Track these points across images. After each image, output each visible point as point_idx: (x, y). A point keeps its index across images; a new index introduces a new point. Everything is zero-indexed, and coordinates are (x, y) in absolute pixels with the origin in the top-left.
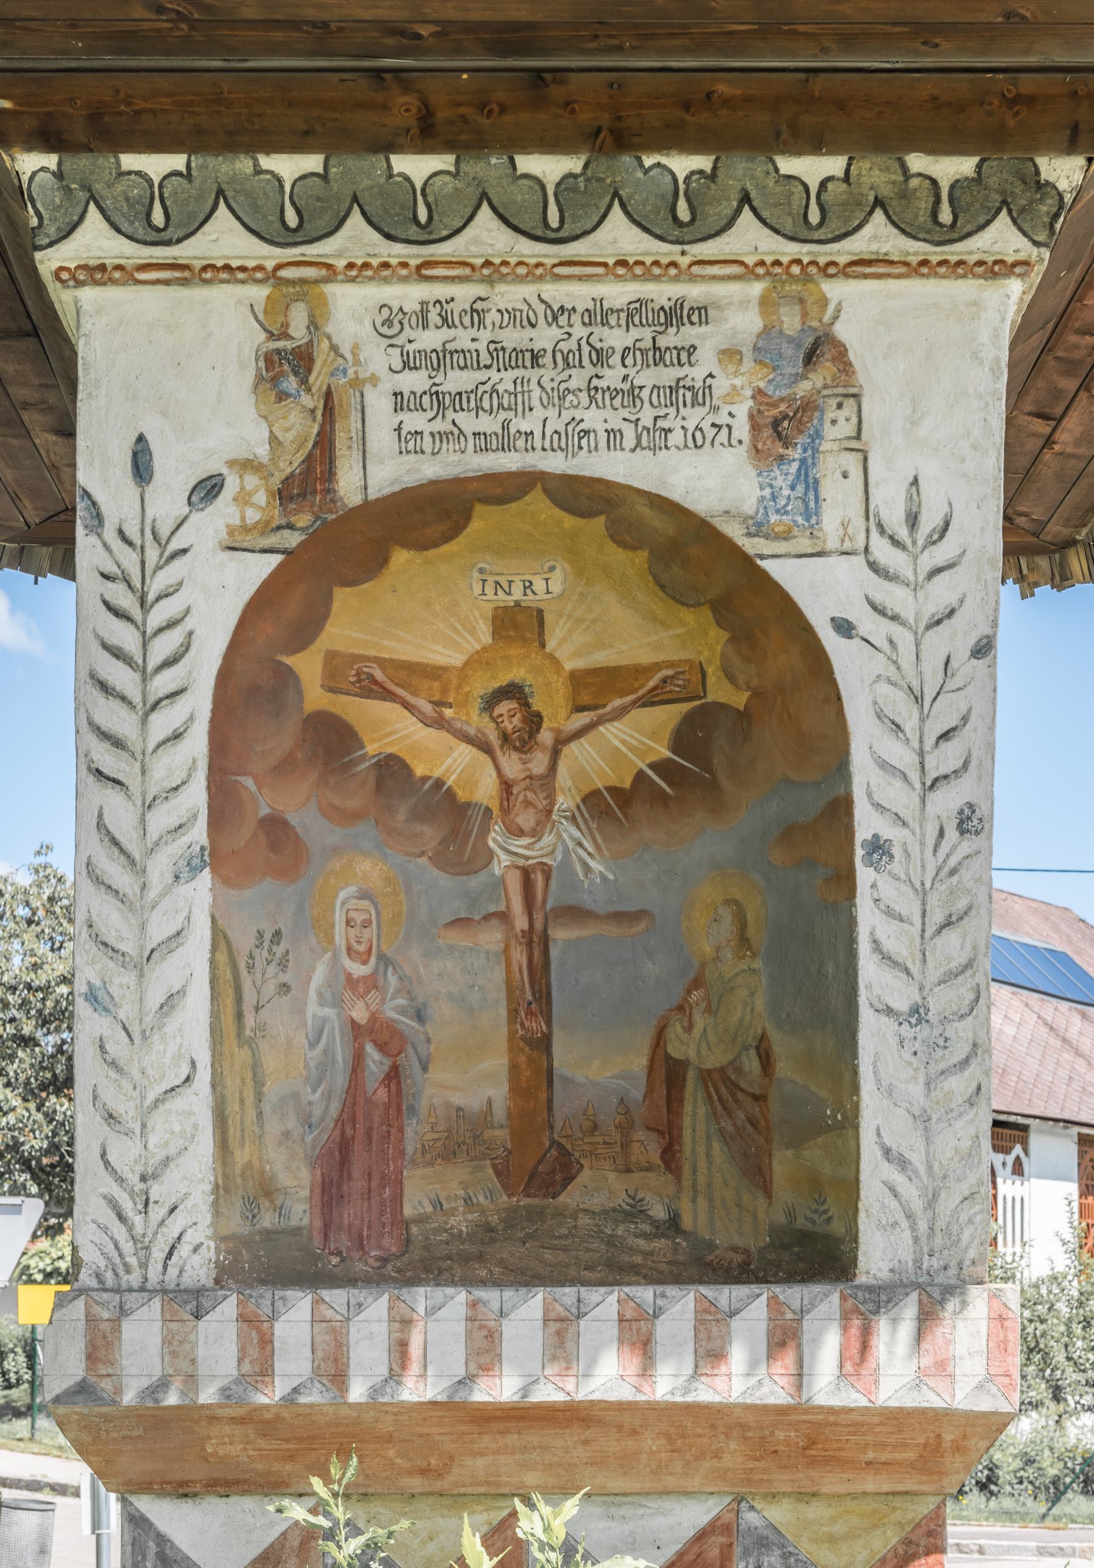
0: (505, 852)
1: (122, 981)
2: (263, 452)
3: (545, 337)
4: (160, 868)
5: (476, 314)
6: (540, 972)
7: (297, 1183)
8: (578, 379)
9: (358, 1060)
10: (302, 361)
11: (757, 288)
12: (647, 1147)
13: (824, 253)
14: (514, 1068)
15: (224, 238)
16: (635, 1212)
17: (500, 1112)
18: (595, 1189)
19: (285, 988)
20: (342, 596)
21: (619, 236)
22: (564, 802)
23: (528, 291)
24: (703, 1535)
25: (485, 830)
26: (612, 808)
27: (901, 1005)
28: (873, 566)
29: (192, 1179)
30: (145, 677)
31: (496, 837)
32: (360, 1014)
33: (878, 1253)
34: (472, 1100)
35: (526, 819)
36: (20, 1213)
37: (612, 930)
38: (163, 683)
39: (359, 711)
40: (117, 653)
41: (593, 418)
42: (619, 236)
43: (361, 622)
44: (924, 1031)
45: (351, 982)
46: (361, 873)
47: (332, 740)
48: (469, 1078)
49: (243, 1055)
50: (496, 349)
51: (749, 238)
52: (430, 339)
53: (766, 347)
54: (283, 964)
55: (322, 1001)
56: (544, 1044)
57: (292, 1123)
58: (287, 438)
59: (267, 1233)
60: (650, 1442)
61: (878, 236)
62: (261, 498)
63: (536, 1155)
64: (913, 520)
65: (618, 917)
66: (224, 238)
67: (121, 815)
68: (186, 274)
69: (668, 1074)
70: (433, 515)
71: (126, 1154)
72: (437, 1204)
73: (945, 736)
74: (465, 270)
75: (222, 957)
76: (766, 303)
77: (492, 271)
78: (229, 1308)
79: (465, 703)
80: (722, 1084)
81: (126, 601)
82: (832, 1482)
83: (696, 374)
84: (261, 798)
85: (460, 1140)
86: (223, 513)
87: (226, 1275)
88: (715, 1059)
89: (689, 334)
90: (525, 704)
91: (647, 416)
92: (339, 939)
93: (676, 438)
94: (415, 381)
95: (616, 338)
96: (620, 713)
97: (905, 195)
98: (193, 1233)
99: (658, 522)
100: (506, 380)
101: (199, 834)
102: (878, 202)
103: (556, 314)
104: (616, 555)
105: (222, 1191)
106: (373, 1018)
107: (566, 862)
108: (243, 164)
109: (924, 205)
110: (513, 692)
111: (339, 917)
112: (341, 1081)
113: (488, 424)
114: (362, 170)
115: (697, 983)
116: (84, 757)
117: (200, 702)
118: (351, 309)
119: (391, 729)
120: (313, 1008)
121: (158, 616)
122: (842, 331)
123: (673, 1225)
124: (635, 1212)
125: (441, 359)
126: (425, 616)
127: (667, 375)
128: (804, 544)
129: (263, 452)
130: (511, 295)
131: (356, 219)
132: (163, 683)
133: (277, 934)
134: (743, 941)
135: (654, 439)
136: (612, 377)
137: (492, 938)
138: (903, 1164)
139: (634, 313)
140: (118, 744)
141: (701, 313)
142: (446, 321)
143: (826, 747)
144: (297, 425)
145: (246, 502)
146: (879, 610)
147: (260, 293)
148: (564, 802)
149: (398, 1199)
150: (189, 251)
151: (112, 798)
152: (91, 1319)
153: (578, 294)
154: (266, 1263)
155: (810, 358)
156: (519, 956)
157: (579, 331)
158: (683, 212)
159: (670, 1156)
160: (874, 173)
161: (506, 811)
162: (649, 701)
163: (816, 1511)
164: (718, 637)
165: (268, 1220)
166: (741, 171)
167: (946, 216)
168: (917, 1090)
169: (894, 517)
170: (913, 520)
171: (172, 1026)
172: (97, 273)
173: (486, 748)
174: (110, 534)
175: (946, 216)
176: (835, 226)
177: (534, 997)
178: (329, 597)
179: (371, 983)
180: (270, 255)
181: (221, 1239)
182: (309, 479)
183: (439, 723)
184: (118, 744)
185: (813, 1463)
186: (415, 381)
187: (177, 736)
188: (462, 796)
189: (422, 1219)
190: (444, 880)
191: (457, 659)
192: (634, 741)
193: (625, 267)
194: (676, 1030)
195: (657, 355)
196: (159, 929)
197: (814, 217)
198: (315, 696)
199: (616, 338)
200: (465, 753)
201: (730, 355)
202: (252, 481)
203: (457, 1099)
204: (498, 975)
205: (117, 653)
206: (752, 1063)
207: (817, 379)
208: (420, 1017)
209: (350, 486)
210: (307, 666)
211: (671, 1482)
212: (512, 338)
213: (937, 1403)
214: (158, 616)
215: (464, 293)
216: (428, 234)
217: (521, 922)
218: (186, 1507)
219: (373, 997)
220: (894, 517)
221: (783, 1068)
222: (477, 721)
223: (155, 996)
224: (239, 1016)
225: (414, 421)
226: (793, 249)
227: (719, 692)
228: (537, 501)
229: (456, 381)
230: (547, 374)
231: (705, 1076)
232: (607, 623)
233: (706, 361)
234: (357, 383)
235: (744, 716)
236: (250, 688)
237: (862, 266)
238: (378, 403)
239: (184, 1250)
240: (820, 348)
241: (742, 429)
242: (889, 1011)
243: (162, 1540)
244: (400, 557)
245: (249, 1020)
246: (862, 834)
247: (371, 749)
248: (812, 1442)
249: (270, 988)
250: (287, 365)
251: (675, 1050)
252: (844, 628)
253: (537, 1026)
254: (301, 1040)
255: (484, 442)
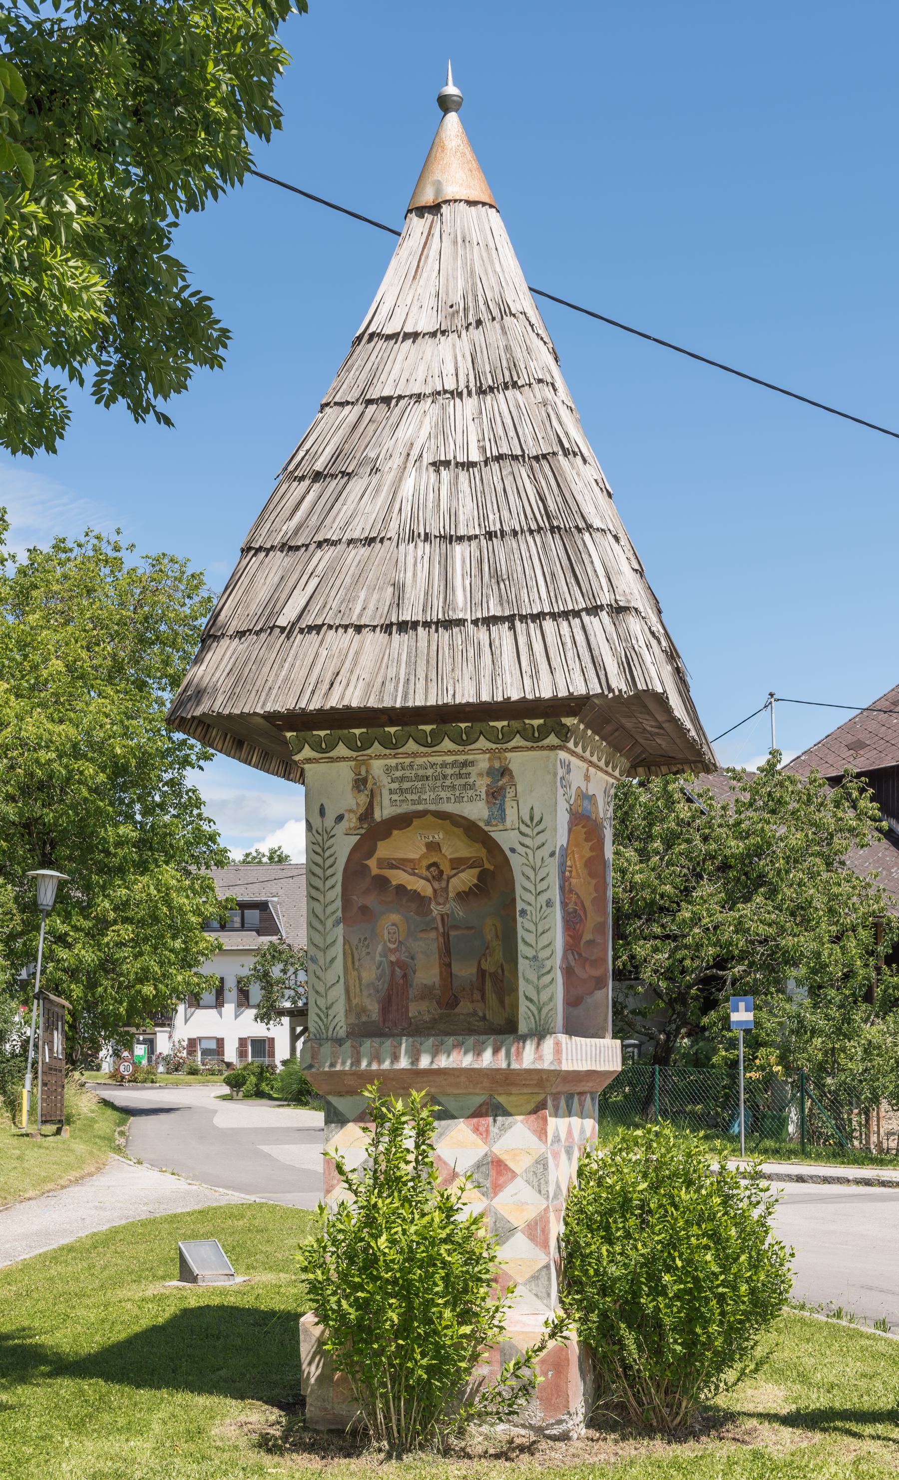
0: (436, 910)
1: (320, 955)
2: (355, 807)
3: (430, 772)
4: (329, 923)
5: (411, 766)
6: (447, 944)
7: (374, 1008)
8: (439, 783)
9: (393, 973)
10: (364, 781)
11: (488, 756)
12: (477, 995)
13: (504, 746)
14: (441, 972)
15: (341, 750)
16: (475, 1014)
17: (437, 985)
18: (465, 1007)
19: (368, 953)
20: (379, 844)
21: (447, 744)
22: (452, 895)
23: (425, 759)
24: (481, 1106)
25: (430, 904)
26: (462, 896)
27: (530, 955)
28: (521, 833)
29: (340, 1008)
30: (324, 871)
31: (433, 906)
32: (393, 959)
33: (523, 1028)
34: (428, 982)
35: (441, 900)
36: (223, 1039)
37: (465, 932)
38: (329, 872)
39: (387, 873)
40: (317, 864)
41: (443, 794)
42: (447, 744)
43: (384, 850)
44: (537, 963)
45: (390, 950)
46: (392, 921)
47: (382, 883)
48: (427, 974)
49: (355, 973)
50: (417, 776)
51: (483, 743)
52: (399, 774)
53: (490, 772)
54: (367, 947)
55: (381, 956)
56: (449, 965)
57: (372, 991)
58: (361, 803)
59: (364, 1023)
60: (463, 1079)
61: (518, 741)
62: (354, 820)
63: (448, 997)
64: (532, 819)
65: (467, 928)
66: (341, 750)
67: (319, 910)
68: (332, 760)
69: (482, 973)
70: (403, 821)
71: (322, 1002)
72: (419, 1013)
73: (542, 880)
74: (408, 755)
75: (347, 947)
76: (490, 759)
77: (415, 755)
78: (348, 1044)
79: (421, 868)
80: (494, 976)
81: (319, 850)
82: (514, 1090)
83: (471, 781)
84: (358, 900)
85: (426, 993)
86: (344, 824)
87: (349, 1035)
88: (492, 970)
89: (469, 769)
90: (438, 868)
91: (457, 793)
92: (386, 938)
93: (465, 799)
94: (395, 786)
95: (449, 771)
96: (463, 871)
97: (525, 729)
98: (340, 1023)
99: (463, 821)
100: (419, 784)
101: (339, 914)
102: (518, 732)
103: (433, 765)
104: (455, 829)
105: (348, 1012)
106: (398, 960)
107: (452, 912)
108: (346, 731)
109: (530, 732)
110: (434, 864)
111: (386, 932)
112: (388, 978)
113: (415, 797)
114: (378, 731)
115: (488, 948)
116: (308, 892)
117: (339, 877)
118: (377, 766)
119: (399, 877)
120: (378, 958)
121: (327, 854)
122: (511, 767)
123: (484, 1018)
124: (475, 1014)
125: (402, 779)
126: (408, 846)
127: (463, 781)
128: (501, 827)
129: (355, 807)
130: (420, 761)
131: (376, 743)
132: (329, 872)
133: (366, 939)
134: (497, 936)
135: (459, 800)
136: (448, 782)
137: (433, 935)
138: (531, 1000)
139: (454, 764)
140: (317, 889)
141: (472, 763)
142: (403, 769)
143: (510, 883)
144: (363, 799)
145: (350, 821)
146: (523, 845)
147: (353, 763)
148: (452, 895)
149: (407, 1011)
150: (332, 754)
151: (316, 904)
152: (312, 1047)
153: (439, 760)
154: (364, 1031)
155: (502, 775)
156: (441, 940)
157: (439, 770)
158: (464, 737)
159: (483, 997)
160: (516, 724)
161: (435, 898)
162: (471, 867)
163: (512, 1098)
164: (484, 851)
165: (364, 1019)
166: (478, 726)
167: (536, 735)
168: (535, 980)
169: (527, 819)
170: (532, 819)
171: (334, 965)
172: (309, 761)
173: (428, 880)
174: (314, 832)
175: (536, 735)
176: (506, 739)
177: (447, 952)
178: (376, 845)
179: (396, 950)
180: (354, 754)
181: (348, 1025)
182: (367, 815)
183: (414, 874)
184: (317, 889)
185: (508, 1085)
186: (395, 786)
187: (333, 887)
188: (422, 894)
189: (415, 1017)
190: (418, 918)
191: (417, 857)
192: (466, 879)
193: (450, 752)
194: (483, 961)
195: (460, 776)
196: (329, 941)
197: (500, 736)
198: (375, 871)
199: (449, 771)
200: (422, 882)
201: (480, 775)
202: (352, 815)
203: (425, 982)
204: (435, 945)
205: (317, 864)
206: (500, 971)
207: (504, 780)
208: (413, 958)
209: (377, 816)
210: (372, 863)
211: (471, 1090)
212: (421, 772)
213: (539, 1067)
214: (327, 854)
215: (408, 761)
216: (395, 747)
217: (441, 930)
218: (341, 1099)
219: (398, 954)
220: (527, 819)
221: (506, 973)
222: (425, 873)
223: (329, 959)
224: (353, 963)
225: (395, 797)
226: (494, 746)
227: (487, 865)
228: (429, 817)
229: (406, 785)
230: (430, 782)
231: (490, 974)
232: (455, 847)
233: (473, 775)
234: (379, 787)
235: (493, 872)
236: (355, 871)
237: (515, 749)
238: (385, 792)
239: (338, 1028)
240: (505, 771)
241: (484, 796)
242: (527, 958)
243: (335, 1108)
244: (395, 832)
245: (357, 963)
246: (518, 908)
247: (394, 883)
248: (506, 1079)
249: (364, 953)
250: (360, 783)
251: (483, 967)
252: (513, 850)
253: (447, 960)
254: (374, 967)
255: (414, 802)
